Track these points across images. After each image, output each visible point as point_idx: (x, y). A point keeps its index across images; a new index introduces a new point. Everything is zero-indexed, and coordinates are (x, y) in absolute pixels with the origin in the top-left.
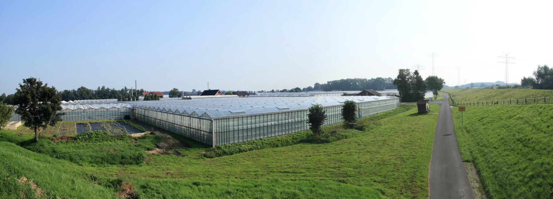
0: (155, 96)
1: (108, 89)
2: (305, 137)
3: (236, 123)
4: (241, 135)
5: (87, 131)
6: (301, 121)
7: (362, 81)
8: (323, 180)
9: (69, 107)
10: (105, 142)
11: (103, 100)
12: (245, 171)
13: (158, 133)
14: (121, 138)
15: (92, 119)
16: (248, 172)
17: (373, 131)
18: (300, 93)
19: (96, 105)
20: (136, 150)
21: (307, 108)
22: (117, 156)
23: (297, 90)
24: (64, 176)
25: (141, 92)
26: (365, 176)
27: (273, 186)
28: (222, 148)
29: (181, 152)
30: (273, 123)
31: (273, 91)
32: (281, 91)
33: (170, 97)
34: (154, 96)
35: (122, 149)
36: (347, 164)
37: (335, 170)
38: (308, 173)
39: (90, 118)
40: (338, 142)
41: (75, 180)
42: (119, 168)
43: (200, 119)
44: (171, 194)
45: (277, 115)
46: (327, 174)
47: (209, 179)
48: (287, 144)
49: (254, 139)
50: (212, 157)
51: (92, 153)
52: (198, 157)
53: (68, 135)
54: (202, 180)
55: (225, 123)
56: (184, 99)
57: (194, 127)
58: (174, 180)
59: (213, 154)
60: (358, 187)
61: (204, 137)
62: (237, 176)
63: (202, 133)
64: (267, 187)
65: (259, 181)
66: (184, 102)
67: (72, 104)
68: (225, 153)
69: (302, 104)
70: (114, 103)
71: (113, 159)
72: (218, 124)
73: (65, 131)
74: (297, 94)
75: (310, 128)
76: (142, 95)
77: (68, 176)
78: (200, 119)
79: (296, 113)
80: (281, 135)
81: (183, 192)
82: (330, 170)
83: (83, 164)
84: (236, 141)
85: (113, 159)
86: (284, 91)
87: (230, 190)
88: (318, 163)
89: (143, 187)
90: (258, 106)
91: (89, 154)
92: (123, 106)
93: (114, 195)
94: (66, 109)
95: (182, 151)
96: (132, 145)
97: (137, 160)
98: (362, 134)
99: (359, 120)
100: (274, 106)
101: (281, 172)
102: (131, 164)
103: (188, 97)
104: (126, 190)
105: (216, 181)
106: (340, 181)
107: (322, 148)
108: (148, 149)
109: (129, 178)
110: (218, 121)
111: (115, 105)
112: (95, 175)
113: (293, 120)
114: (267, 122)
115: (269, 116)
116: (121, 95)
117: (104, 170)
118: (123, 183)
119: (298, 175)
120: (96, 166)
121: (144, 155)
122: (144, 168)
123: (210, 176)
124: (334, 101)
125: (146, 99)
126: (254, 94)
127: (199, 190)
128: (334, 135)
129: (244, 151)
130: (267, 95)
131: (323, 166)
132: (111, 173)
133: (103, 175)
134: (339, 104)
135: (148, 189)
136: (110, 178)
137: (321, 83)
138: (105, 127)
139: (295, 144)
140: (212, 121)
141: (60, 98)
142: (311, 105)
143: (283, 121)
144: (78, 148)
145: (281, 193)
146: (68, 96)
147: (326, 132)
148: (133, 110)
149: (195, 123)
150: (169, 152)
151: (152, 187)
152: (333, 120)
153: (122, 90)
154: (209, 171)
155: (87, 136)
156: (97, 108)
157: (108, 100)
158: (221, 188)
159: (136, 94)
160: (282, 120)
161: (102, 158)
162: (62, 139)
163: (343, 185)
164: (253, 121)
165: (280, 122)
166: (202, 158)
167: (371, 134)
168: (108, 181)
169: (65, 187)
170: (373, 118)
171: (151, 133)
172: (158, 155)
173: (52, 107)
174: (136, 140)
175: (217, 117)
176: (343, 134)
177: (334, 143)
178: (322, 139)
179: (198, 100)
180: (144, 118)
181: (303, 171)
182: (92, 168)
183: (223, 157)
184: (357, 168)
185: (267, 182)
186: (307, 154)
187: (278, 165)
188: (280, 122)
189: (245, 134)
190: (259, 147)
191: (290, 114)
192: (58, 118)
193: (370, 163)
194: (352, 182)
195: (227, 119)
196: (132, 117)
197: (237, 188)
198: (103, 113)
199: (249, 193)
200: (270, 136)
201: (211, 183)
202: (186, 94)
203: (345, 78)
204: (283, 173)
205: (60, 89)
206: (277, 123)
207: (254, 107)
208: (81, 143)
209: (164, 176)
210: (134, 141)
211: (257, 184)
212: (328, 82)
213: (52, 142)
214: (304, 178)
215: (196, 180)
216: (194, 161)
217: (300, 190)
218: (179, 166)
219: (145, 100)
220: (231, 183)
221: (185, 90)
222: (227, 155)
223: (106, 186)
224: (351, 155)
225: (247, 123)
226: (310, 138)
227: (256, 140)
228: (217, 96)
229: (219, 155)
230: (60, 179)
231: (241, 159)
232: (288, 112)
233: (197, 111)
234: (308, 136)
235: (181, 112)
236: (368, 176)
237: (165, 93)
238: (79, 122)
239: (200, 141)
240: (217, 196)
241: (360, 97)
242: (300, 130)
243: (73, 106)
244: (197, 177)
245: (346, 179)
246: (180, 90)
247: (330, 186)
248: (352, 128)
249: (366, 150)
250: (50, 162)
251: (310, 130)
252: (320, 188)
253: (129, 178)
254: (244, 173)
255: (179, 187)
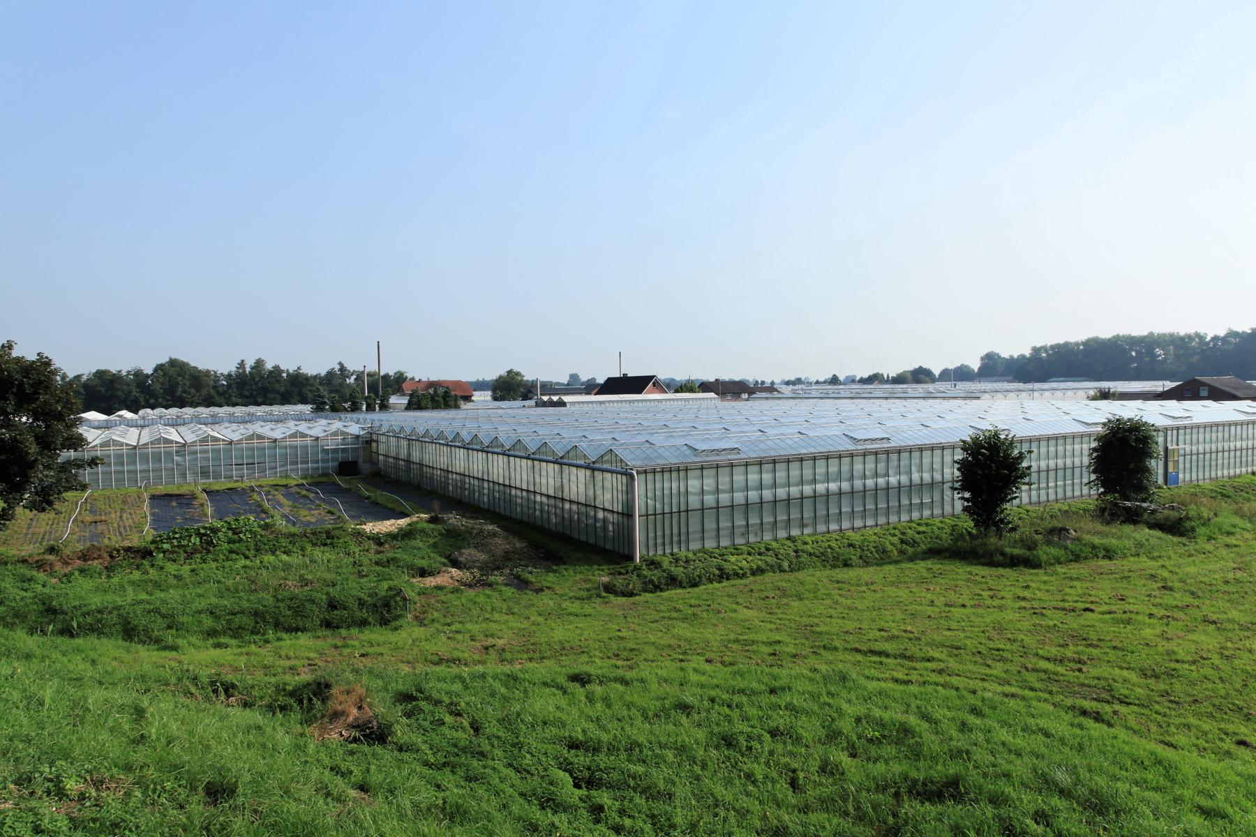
0: (446, 395)
1: (277, 371)
2: (946, 539)
3: (709, 483)
4: (725, 523)
5: (193, 520)
6: (932, 484)
7: (1180, 344)
8: (1013, 696)
9: (116, 435)
10: (269, 558)
11: (260, 410)
12: (737, 641)
13: (454, 519)
14: (328, 539)
15: (217, 476)
16: (746, 643)
17: (1231, 540)
18: (931, 387)
19: (231, 427)
20: (381, 578)
21: (955, 438)
22: (312, 601)
23: (920, 375)
24: (95, 696)
25: (396, 383)
26: (1198, 715)
27: (829, 694)
28: (665, 565)
29: (531, 578)
30: (833, 486)
31: (834, 380)
32: (863, 381)
33: (495, 399)
34: (442, 396)
35: (329, 576)
36: (1112, 655)
37: (1060, 669)
38: (952, 663)
39: (205, 473)
40: (1074, 569)
41: (146, 704)
42: (320, 643)
43: (593, 470)
44: (500, 715)
45: (846, 461)
46: (1031, 678)
47: (620, 663)
48: (882, 557)
49: (768, 537)
50: (631, 595)
51: (214, 600)
52: (584, 594)
53: (115, 541)
54: (597, 666)
55: (672, 484)
56: (542, 404)
57: (574, 498)
58: (507, 668)
59: (635, 582)
60: (1161, 750)
61: (605, 528)
62: (712, 656)
63: (600, 515)
64: (812, 695)
65: (784, 674)
66: (542, 417)
67: (130, 424)
68: (673, 581)
69: (937, 424)
70: (299, 418)
71: (298, 611)
72: (650, 487)
73: (100, 527)
74: (920, 388)
75: (965, 509)
76: (399, 390)
77: (117, 696)
78: (593, 470)
79: (916, 455)
80: (864, 527)
81: (538, 705)
82: (1043, 664)
83: (179, 642)
84: (710, 544)
85: (298, 611)
86: (874, 379)
87: (689, 699)
88: (993, 634)
89: (406, 697)
90: (784, 430)
91: (202, 604)
92: (352, 425)
93: (302, 735)
94: (105, 444)
95: (534, 575)
96: (366, 561)
97: (385, 611)
98: (1181, 550)
99: (1165, 493)
100: (836, 431)
101: (857, 650)
102: (363, 623)
103: (555, 398)
104: (343, 713)
105: (645, 671)
106: (1084, 713)
107: (1008, 581)
108: (423, 573)
109: (356, 671)
110: (650, 476)
111: (303, 427)
112: (230, 678)
113: (904, 479)
114: (814, 481)
115: (821, 464)
116: (324, 391)
117: (265, 654)
118: (334, 691)
119: (918, 665)
120: (234, 642)
121: (410, 593)
122: (408, 634)
123: (625, 654)
124: (1065, 417)
125: (416, 404)
126: (771, 389)
127: (590, 699)
128: (1053, 542)
129: (737, 574)
130: (814, 394)
131: (1015, 647)
132: (287, 663)
133: (259, 674)
134: (1081, 429)
135: (423, 704)
136: (288, 678)
137: (1005, 354)
138: (266, 505)
139: (911, 559)
140: (632, 476)
141: (78, 402)
142: (971, 432)
143: (870, 483)
144: (157, 585)
145: (858, 720)
146: (109, 392)
147: (1025, 530)
148: (368, 442)
149: (577, 485)
150: (492, 578)
151: (436, 695)
152: (1059, 485)
153: (331, 374)
154: (622, 638)
155: (195, 540)
156: (235, 437)
157: (277, 409)
158: (661, 693)
159: (379, 390)
160: (865, 477)
161: (256, 614)
162: (84, 557)
163: (1096, 729)
164: (767, 477)
165: (858, 484)
166: (599, 596)
167: (1223, 552)
168: (277, 687)
169: (104, 736)
170: (1230, 491)
171: (433, 520)
172: (455, 591)
173: (37, 438)
174: (381, 544)
175: (649, 465)
176: (1097, 540)
177: (1059, 569)
178: (1008, 550)
179: (586, 408)
180: (408, 470)
181: (936, 655)
182: (216, 653)
183: (665, 594)
184: (1156, 677)
185: (811, 680)
186: (952, 597)
187: (850, 626)
188: (858, 484)
189: (740, 522)
190: (785, 564)
191: (894, 457)
192: (68, 479)
193: (1217, 668)
194: (1132, 722)
195: (681, 470)
196: (365, 467)
197: (713, 693)
198: (258, 454)
199: (752, 712)
200: (821, 528)
201: (629, 675)
202: (548, 388)
203: (1106, 333)
204: (865, 653)
205: (75, 363)
206: (845, 486)
207: (771, 432)
208: (171, 568)
209: (476, 657)
210: (374, 547)
211: (776, 684)
212: (1036, 350)
213: (41, 576)
214: (940, 679)
215: (582, 667)
216: (575, 607)
217: (925, 717)
218: (526, 624)
219: (409, 407)
220: (694, 678)
221: (544, 376)
222: (681, 586)
223: (270, 708)
224: (1129, 622)
225: (747, 486)
226: (965, 545)
227: (776, 540)
228: (649, 395)
229: (654, 587)
230: (78, 713)
231: (726, 602)
232: (887, 452)
233: (583, 445)
234: (957, 535)
235: (532, 448)
236: (1211, 716)
237: (480, 386)
238: (161, 490)
239: (592, 541)
240: (646, 717)
241: (1175, 408)
242: (927, 513)
243: (134, 432)
244: (585, 658)
245: (1108, 708)
246: (528, 376)
247: (1042, 723)
248: (1135, 522)
249: (1198, 614)
250: (28, 657)
251: (965, 516)
252: (1003, 723)
253: (356, 671)
254: (735, 646)
255: (526, 691)
